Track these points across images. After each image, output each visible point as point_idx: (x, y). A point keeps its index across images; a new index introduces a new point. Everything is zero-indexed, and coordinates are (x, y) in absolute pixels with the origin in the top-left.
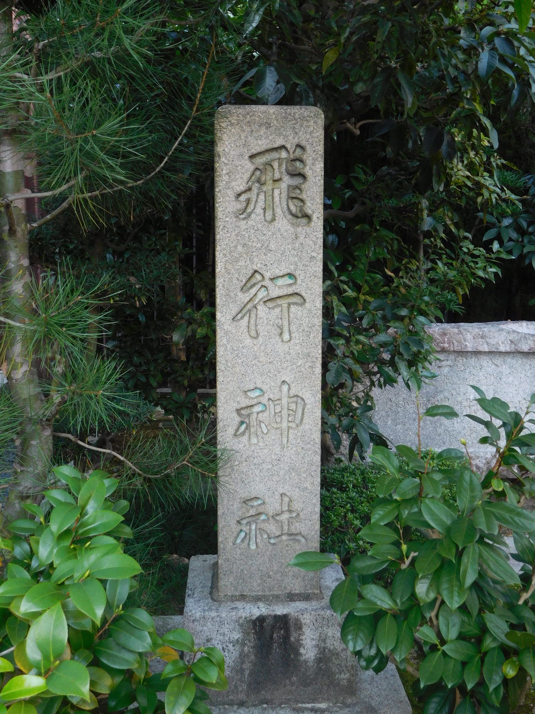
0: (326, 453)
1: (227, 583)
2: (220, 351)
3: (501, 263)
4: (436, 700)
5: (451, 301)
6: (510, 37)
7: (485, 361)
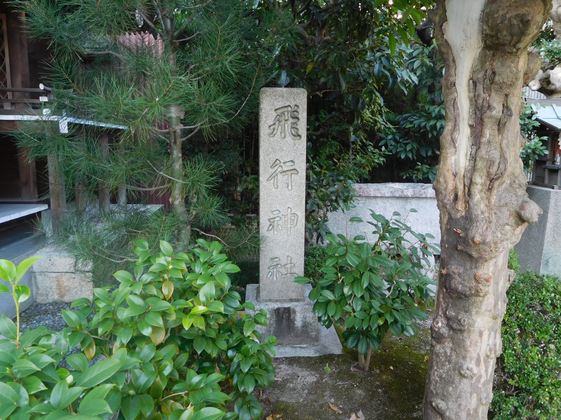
0: (306, 241)
1: (263, 294)
2: (261, 194)
3: (385, 156)
4: (352, 338)
5: (364, 173)
6: (388, 58)
7: (379, 201)
